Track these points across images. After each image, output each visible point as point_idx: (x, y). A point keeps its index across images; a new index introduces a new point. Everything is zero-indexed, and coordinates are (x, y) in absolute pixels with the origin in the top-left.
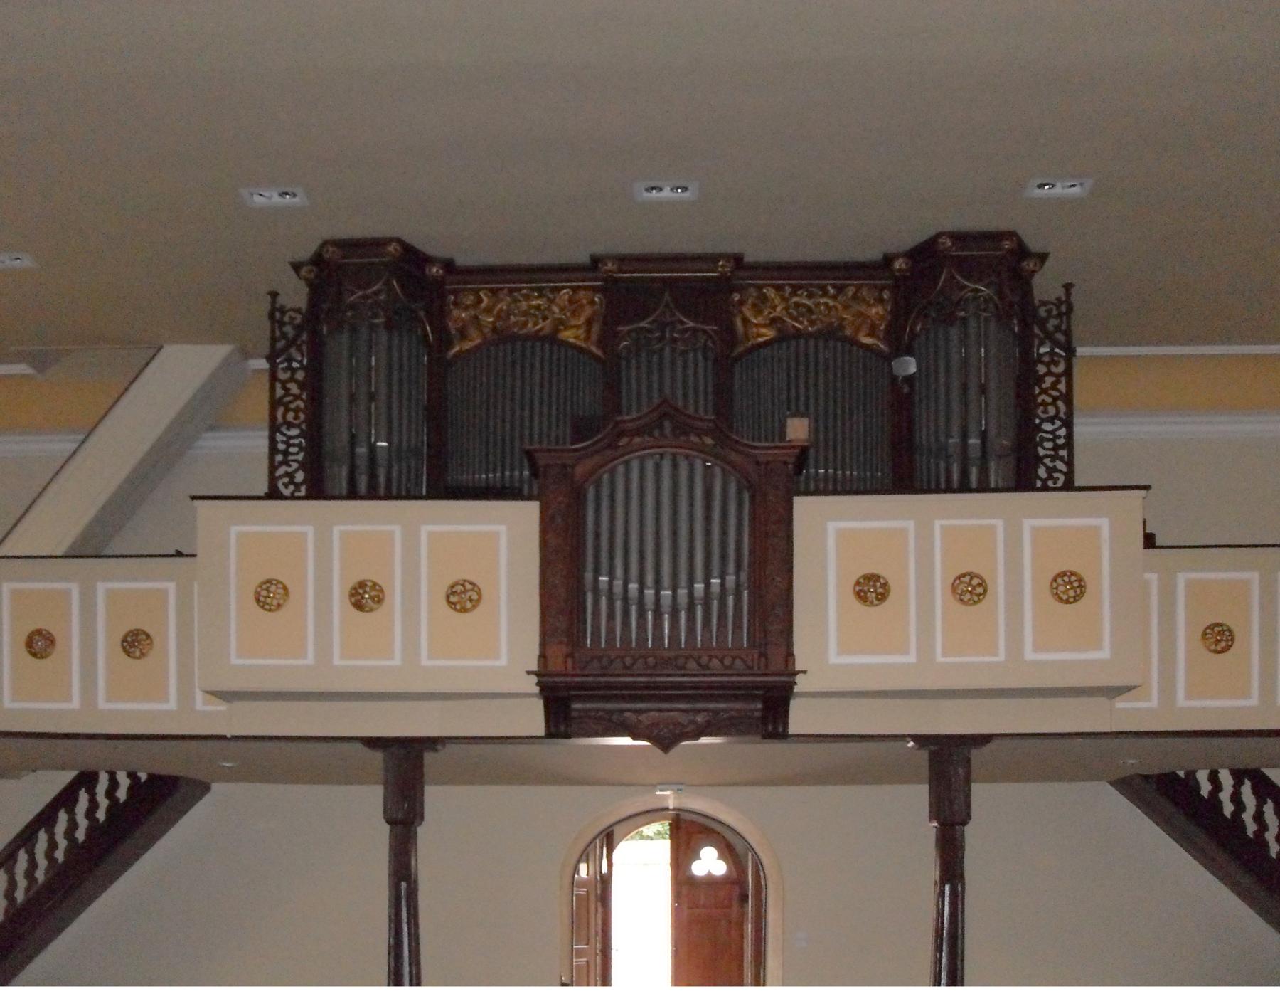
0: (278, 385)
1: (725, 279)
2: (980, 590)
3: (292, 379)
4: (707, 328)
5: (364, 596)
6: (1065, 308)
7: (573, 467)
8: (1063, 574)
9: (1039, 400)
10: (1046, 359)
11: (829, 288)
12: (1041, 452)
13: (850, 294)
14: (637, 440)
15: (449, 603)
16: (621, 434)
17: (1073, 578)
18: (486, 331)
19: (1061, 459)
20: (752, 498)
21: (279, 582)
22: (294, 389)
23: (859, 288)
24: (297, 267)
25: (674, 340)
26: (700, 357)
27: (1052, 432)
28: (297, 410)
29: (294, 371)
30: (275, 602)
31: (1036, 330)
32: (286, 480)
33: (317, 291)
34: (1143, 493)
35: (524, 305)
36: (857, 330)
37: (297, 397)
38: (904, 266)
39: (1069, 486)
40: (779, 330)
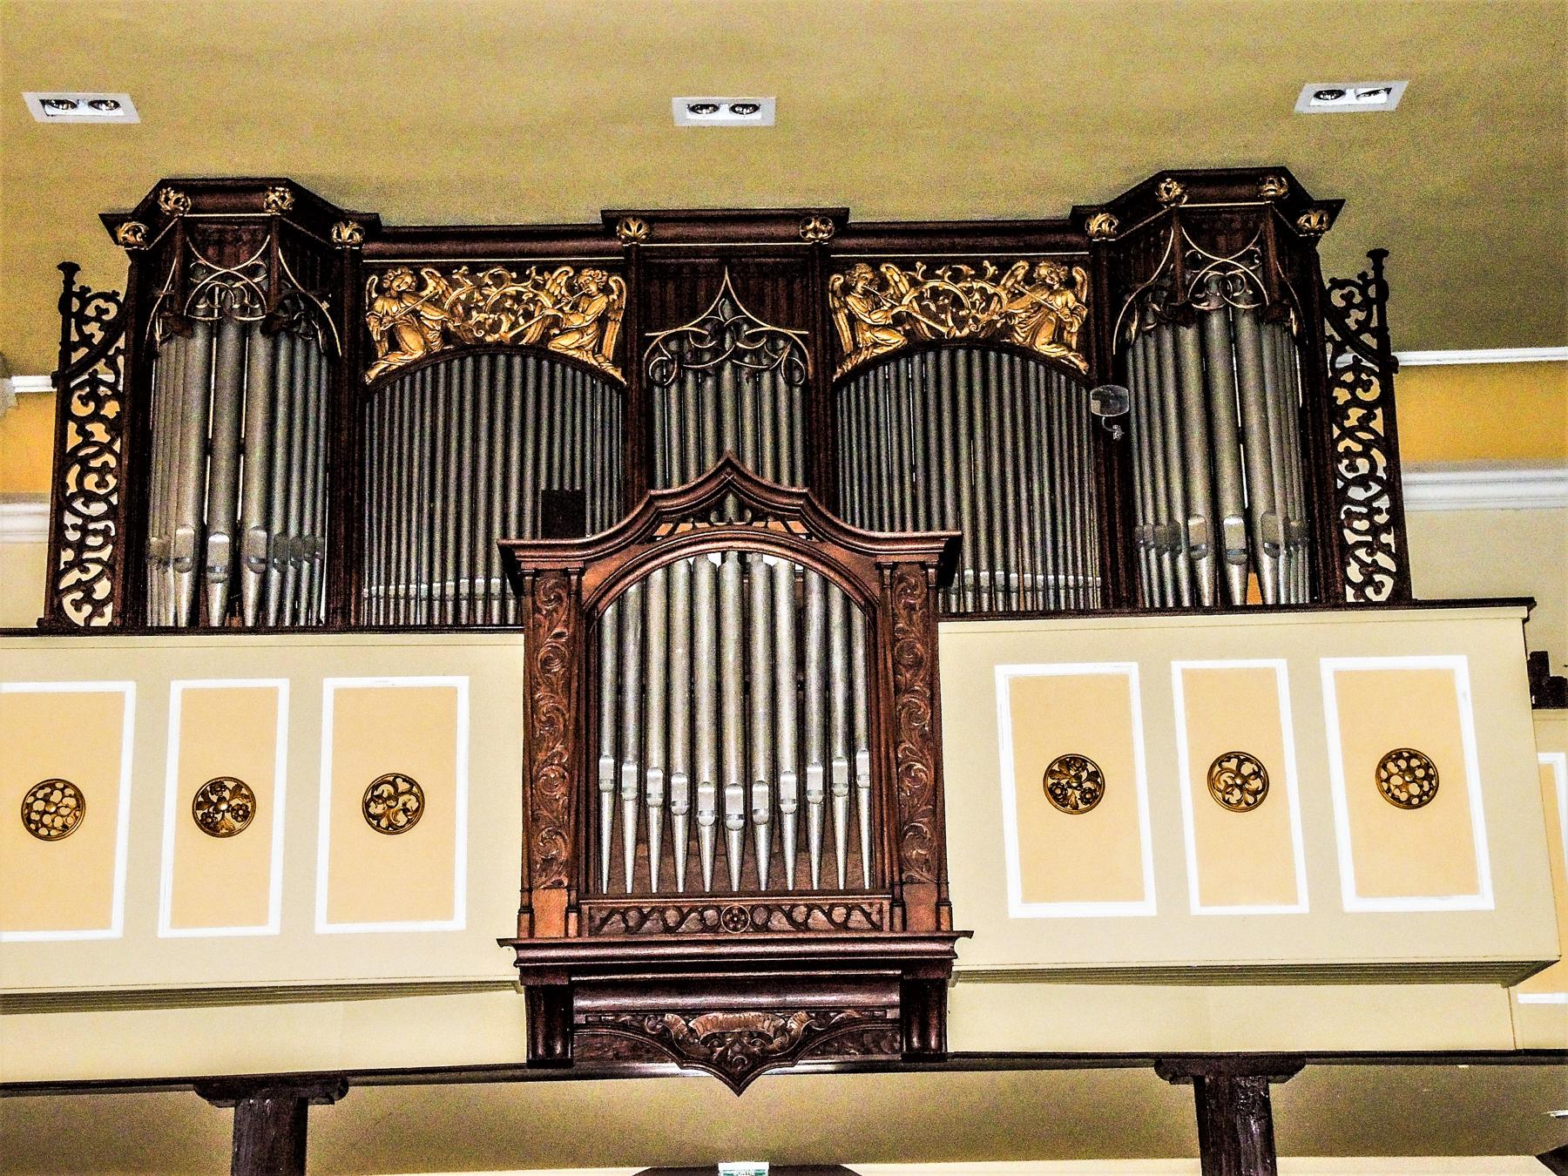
0: (72, 427)
1: (821, 251)
2: (1256, 784)
3: (96, 417)
4: (789, 332)
5: (221, 807)
6: (1374, 286)
7: (582, 572)
8: (1397, 755)
9: (1341, 448)
10: (1349, 377)
11: (986, 263)
12: (1351, 538)
13: (1021, 273)
14: (685, 527)
15: (369, 816)
16: (660, 517)
17: (1414, 763)
18: (430, 336)
19: (1385, 548)
20: (871, 627)
21: (67, 785)
22: (99, 432)
23: (1033, 265)
24: (111, 222)
25: (738, 354)
26: (781, 380)
27: (1367, 502)
28: (104, 470)
29: (100, 401)
30: (59, 822)
31: (1329, 330)
32: (79, 595)
33: (145, 267)
34: (1522, 611)
35: (494, 293)
36: (1035, 332)
37: (105, 448)
38: (1105, 227)
39: (1402, 598)
40: (907, 334)
